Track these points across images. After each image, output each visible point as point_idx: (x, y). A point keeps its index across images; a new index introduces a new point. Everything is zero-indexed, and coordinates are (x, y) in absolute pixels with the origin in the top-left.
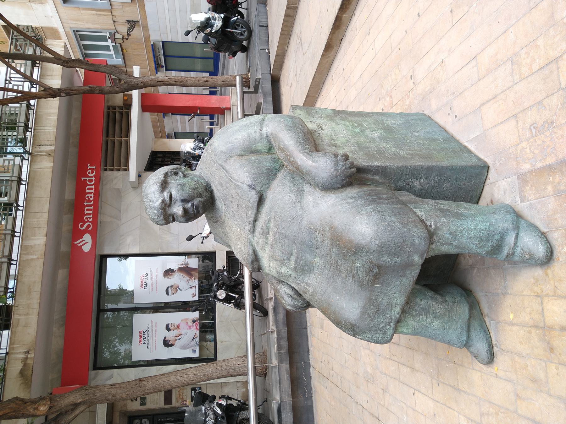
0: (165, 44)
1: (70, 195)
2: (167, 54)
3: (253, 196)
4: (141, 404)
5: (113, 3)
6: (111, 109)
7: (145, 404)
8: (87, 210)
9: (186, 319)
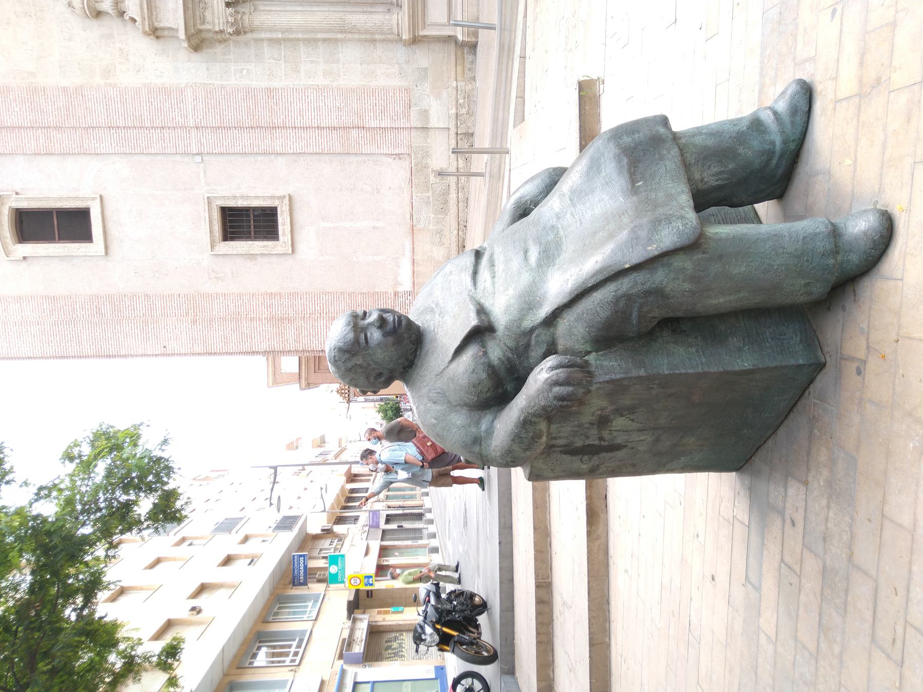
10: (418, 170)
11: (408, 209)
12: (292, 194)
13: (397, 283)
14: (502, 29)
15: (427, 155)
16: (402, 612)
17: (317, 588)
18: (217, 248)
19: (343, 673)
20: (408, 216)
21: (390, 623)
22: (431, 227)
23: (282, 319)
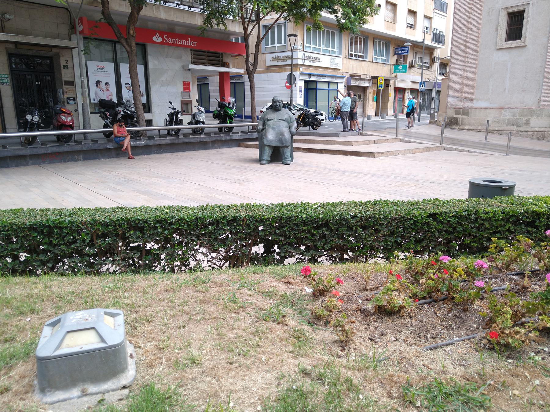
0: (243, 83)
1: (178, 30)
2: (236, 84)
3: (285, 119)
4: (64, 66)
5: (265, 54)
6: (221, 55)
7: (64, 68)
8: (174, 40)
9: (112, 95)
10: (531, 112)
11: (512, 106)
12: (527, 47)
13: (477, 100)
14: (485, 144)
15: (538, 116)
16: (373, 101)
17: (393, 60)
18: (503, 11)
19: (343, 77)
20: (509, 106)
21: (368, 96)
22: (502, 117)
23: (466, 46)
